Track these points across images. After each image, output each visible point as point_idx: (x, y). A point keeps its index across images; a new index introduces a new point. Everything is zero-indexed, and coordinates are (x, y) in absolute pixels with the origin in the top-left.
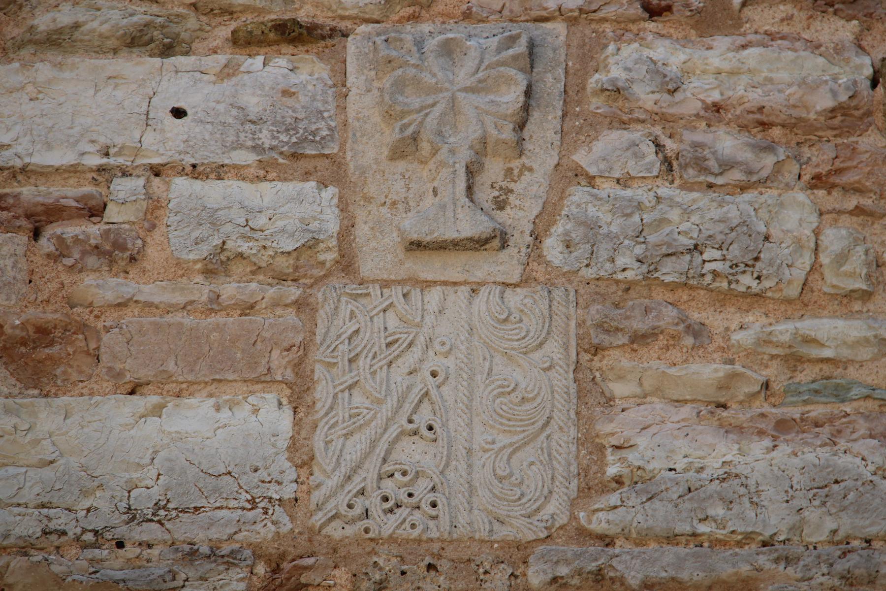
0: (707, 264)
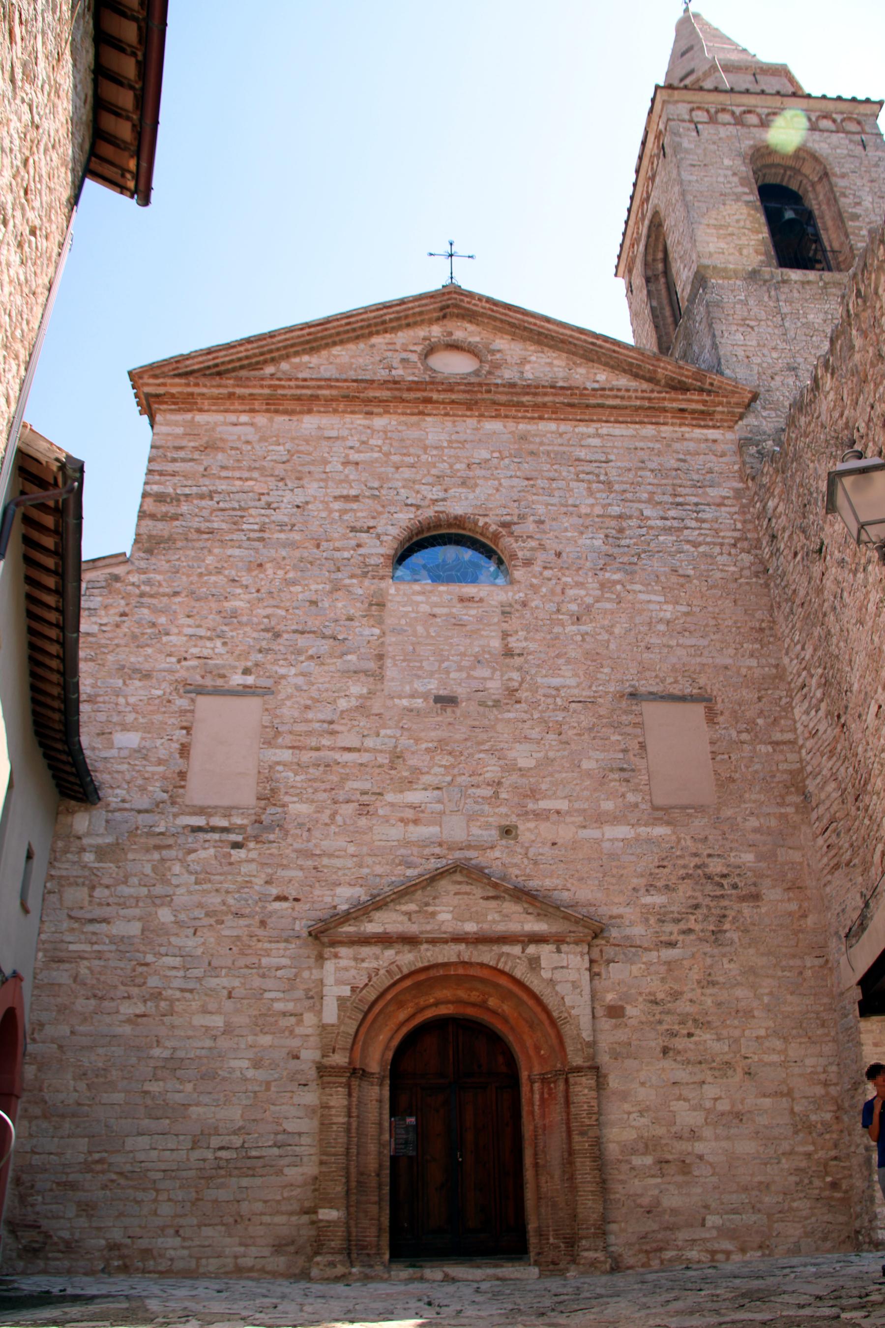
0: (876, 707)
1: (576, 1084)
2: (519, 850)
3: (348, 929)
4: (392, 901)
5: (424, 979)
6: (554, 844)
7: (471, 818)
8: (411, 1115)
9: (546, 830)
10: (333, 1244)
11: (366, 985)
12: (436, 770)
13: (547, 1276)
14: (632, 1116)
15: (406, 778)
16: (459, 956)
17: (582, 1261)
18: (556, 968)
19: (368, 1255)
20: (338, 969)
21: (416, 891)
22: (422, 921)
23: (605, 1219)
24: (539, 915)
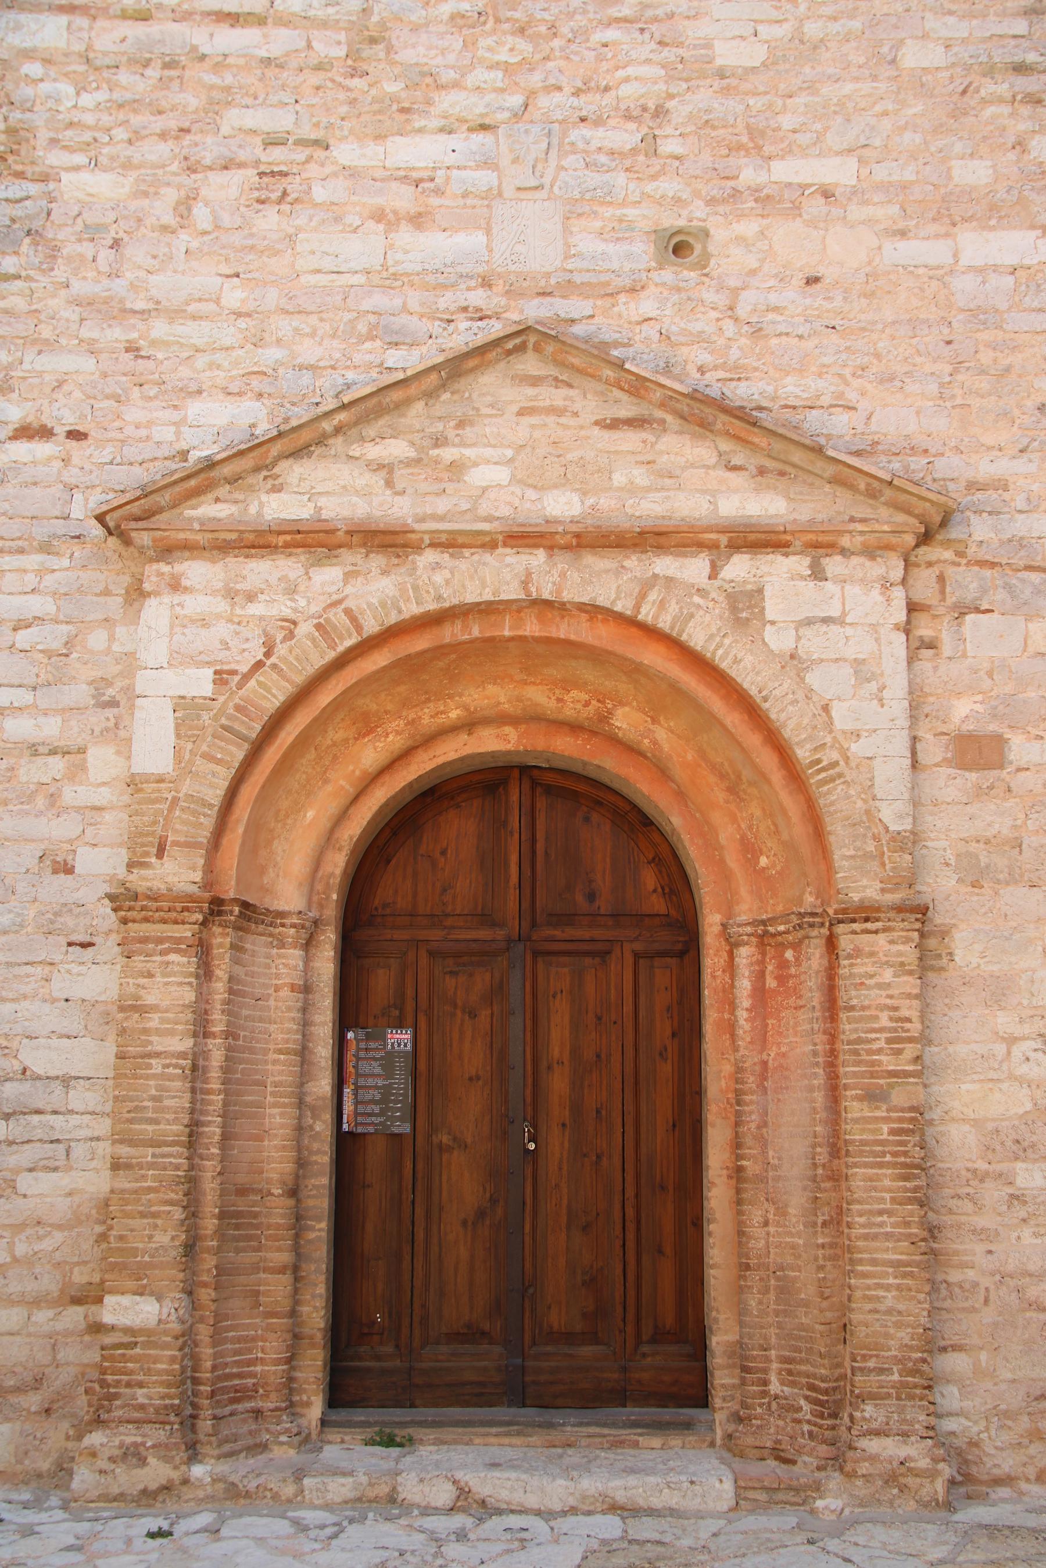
1: (857, 952)
2: (710, 296)
3: (212, 510)
4: (338, 430)
5: (426, 650)
6: (812, 281)
7: (575, 209)
8: (400, 1025)
9: (791, 242)
10: (141, 1395)
11: (259, 665)
12: (481, 76)
13: (757, 1507)
14: (1019, 1050)
15: (394, 99)
16: (525, 584)
17: (864, 1468)
18: (809, 622)
19: (257, 1413)
20: (178, 622)
21: (408, 402)
22: (424, 487)
23: (933, 1344)
24: (762, 471)
